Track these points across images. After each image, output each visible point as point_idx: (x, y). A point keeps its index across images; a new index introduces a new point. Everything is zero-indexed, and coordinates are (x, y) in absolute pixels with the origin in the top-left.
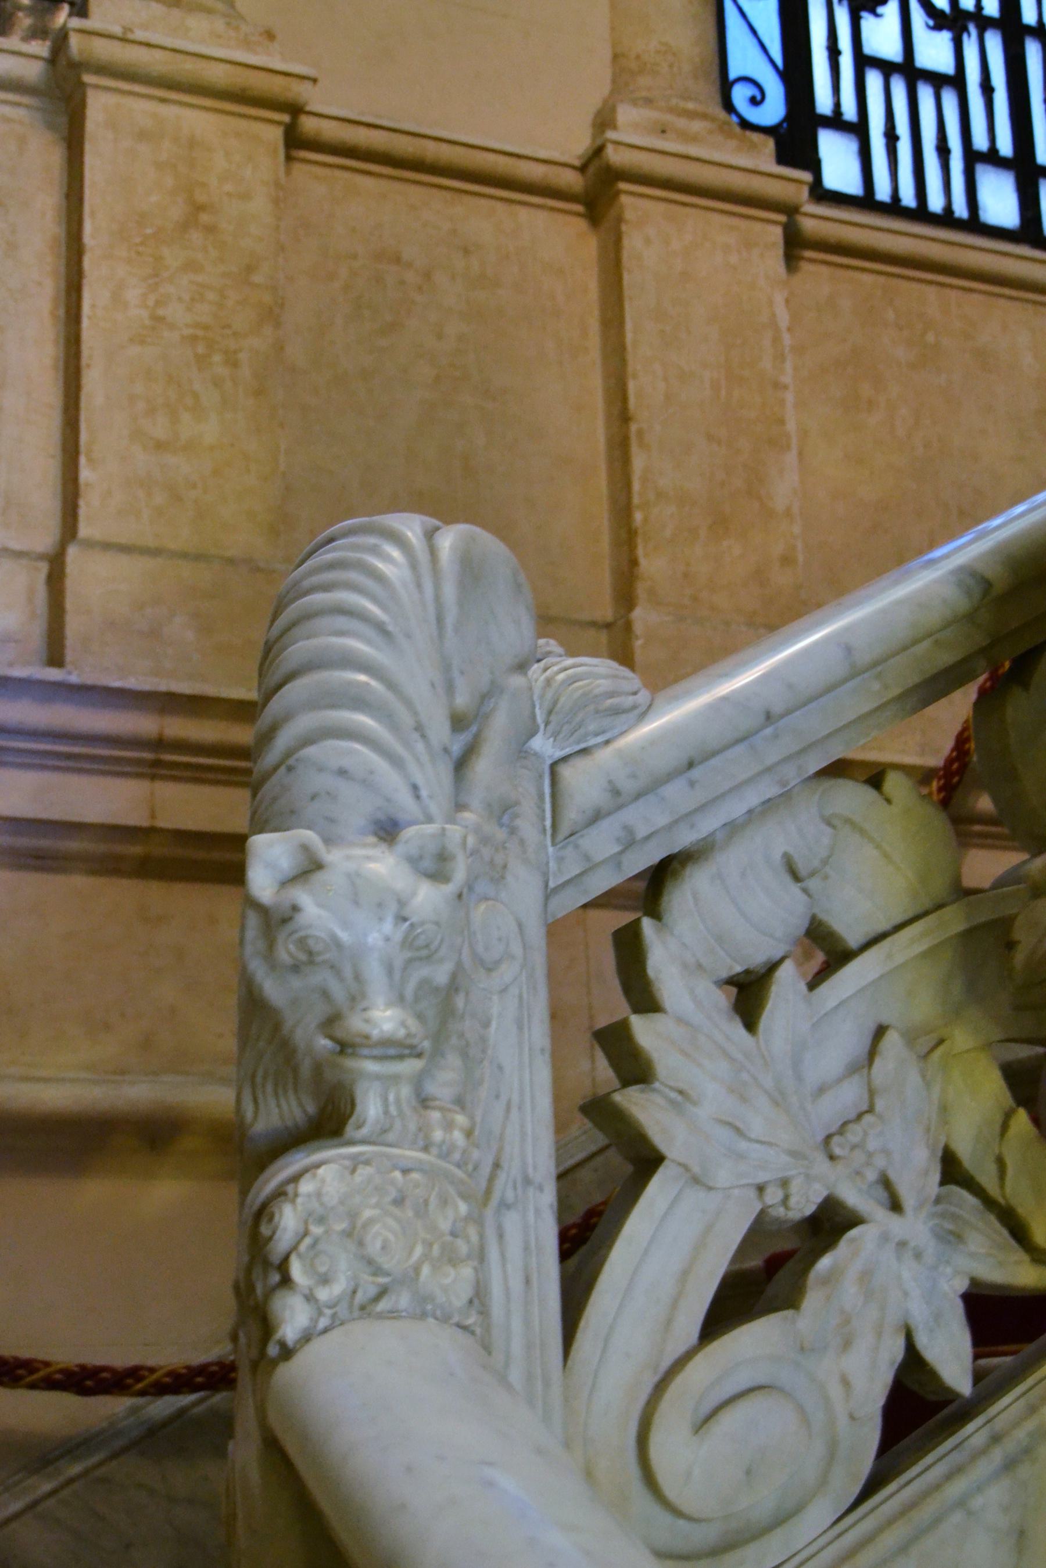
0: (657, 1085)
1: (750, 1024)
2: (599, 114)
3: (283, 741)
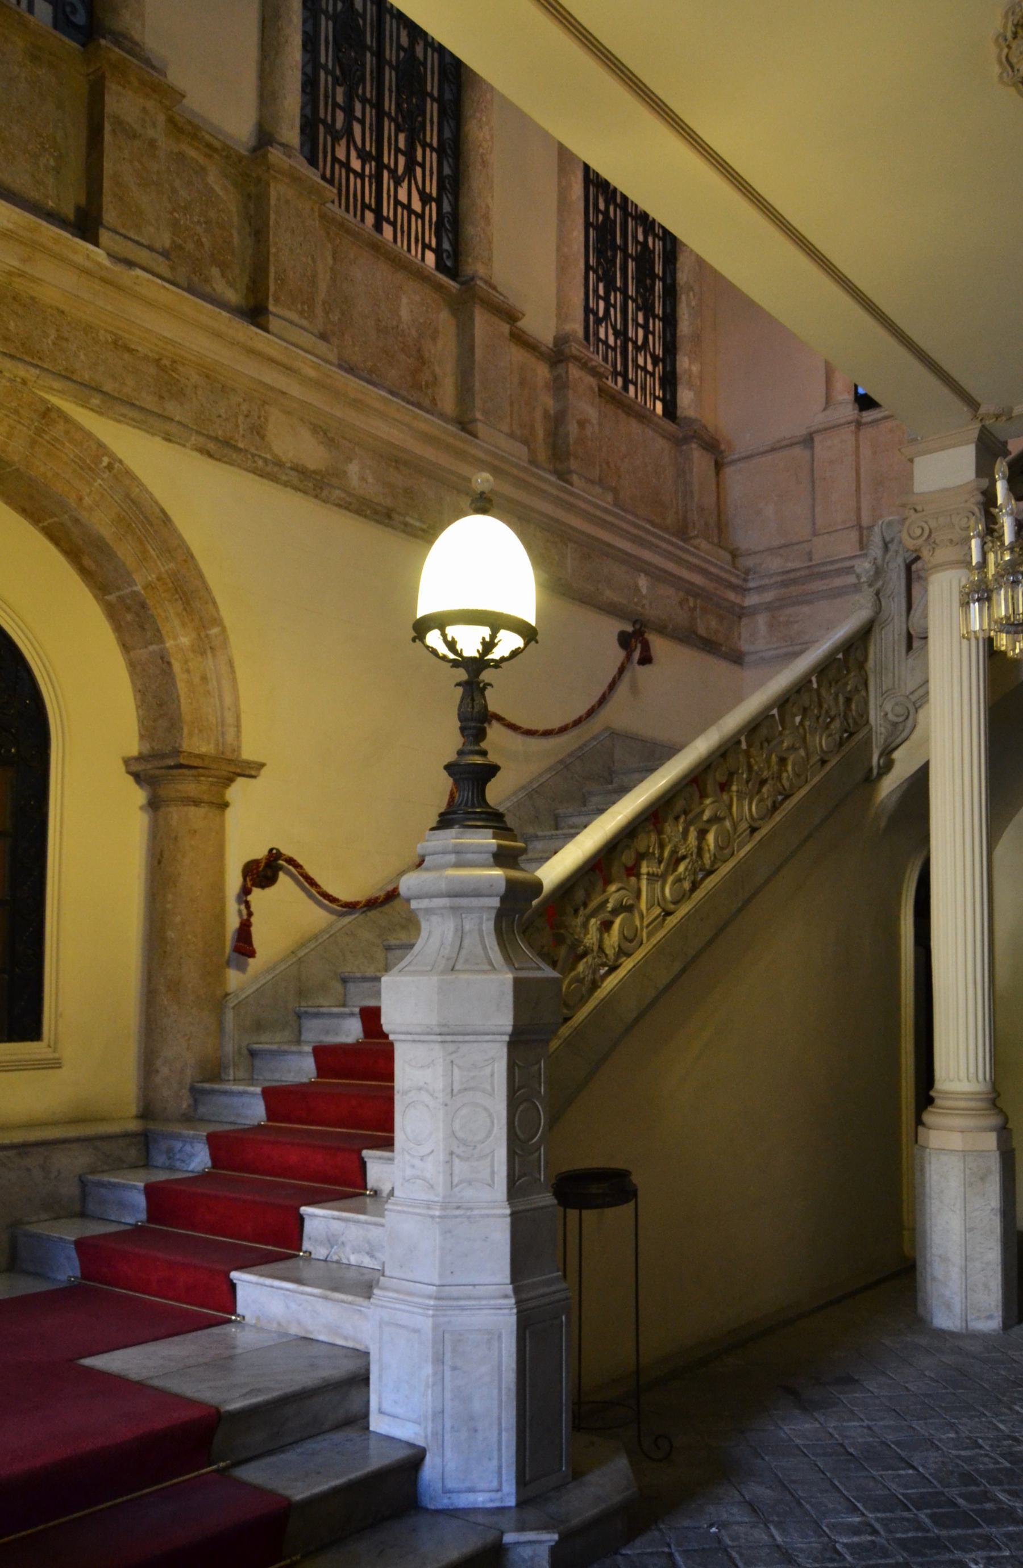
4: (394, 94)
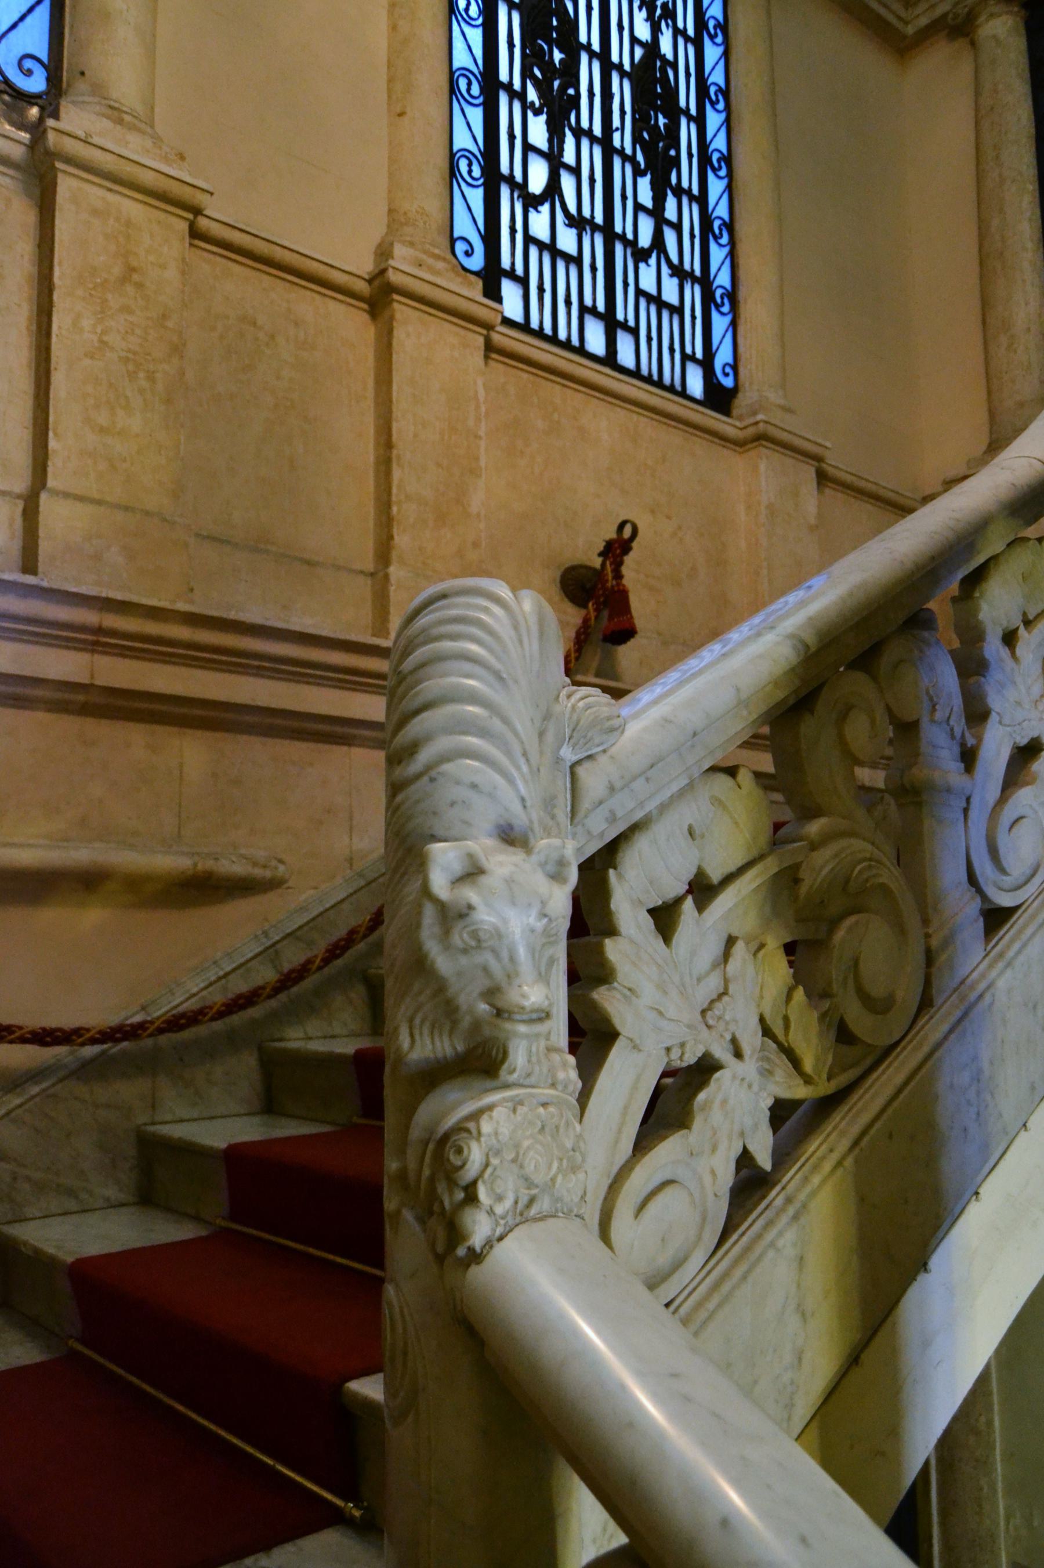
0: (616, 984)
1: (667, 939)
2: (379, 246)
3: (424, 757)
4: (695, 160)
